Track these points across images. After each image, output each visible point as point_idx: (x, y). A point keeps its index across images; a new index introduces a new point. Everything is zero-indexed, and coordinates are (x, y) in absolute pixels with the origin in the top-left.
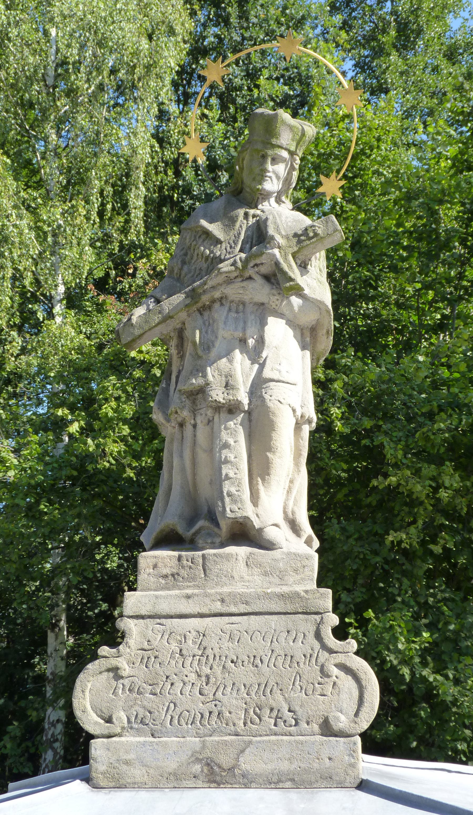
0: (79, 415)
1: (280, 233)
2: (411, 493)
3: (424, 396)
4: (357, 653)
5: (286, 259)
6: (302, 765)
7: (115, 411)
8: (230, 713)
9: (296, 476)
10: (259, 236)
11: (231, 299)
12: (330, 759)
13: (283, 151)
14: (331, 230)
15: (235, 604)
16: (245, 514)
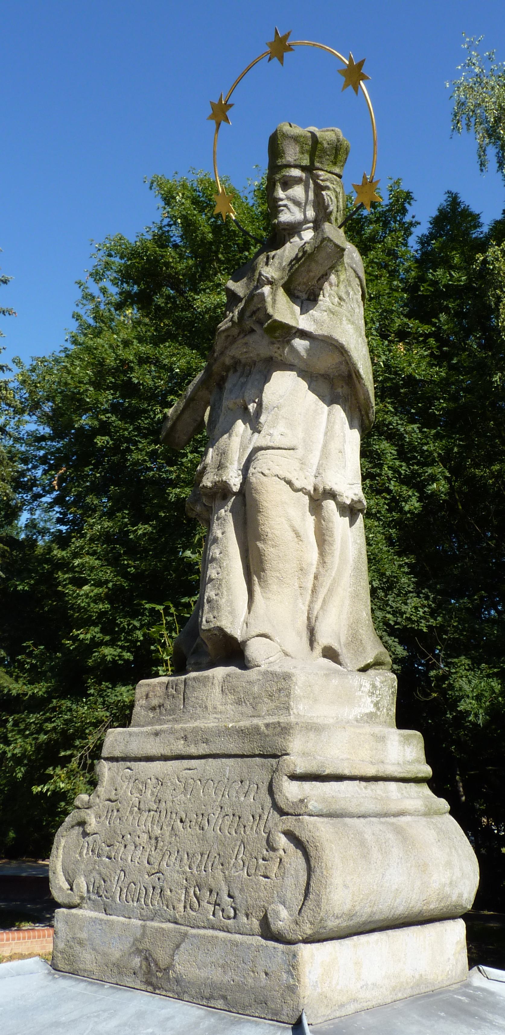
6: (236, 978)
8: (171, 891)
9: (321, 569)
11: (243, 361)
12: (266, 974)
13: (292, 169)
16: (218, 624)
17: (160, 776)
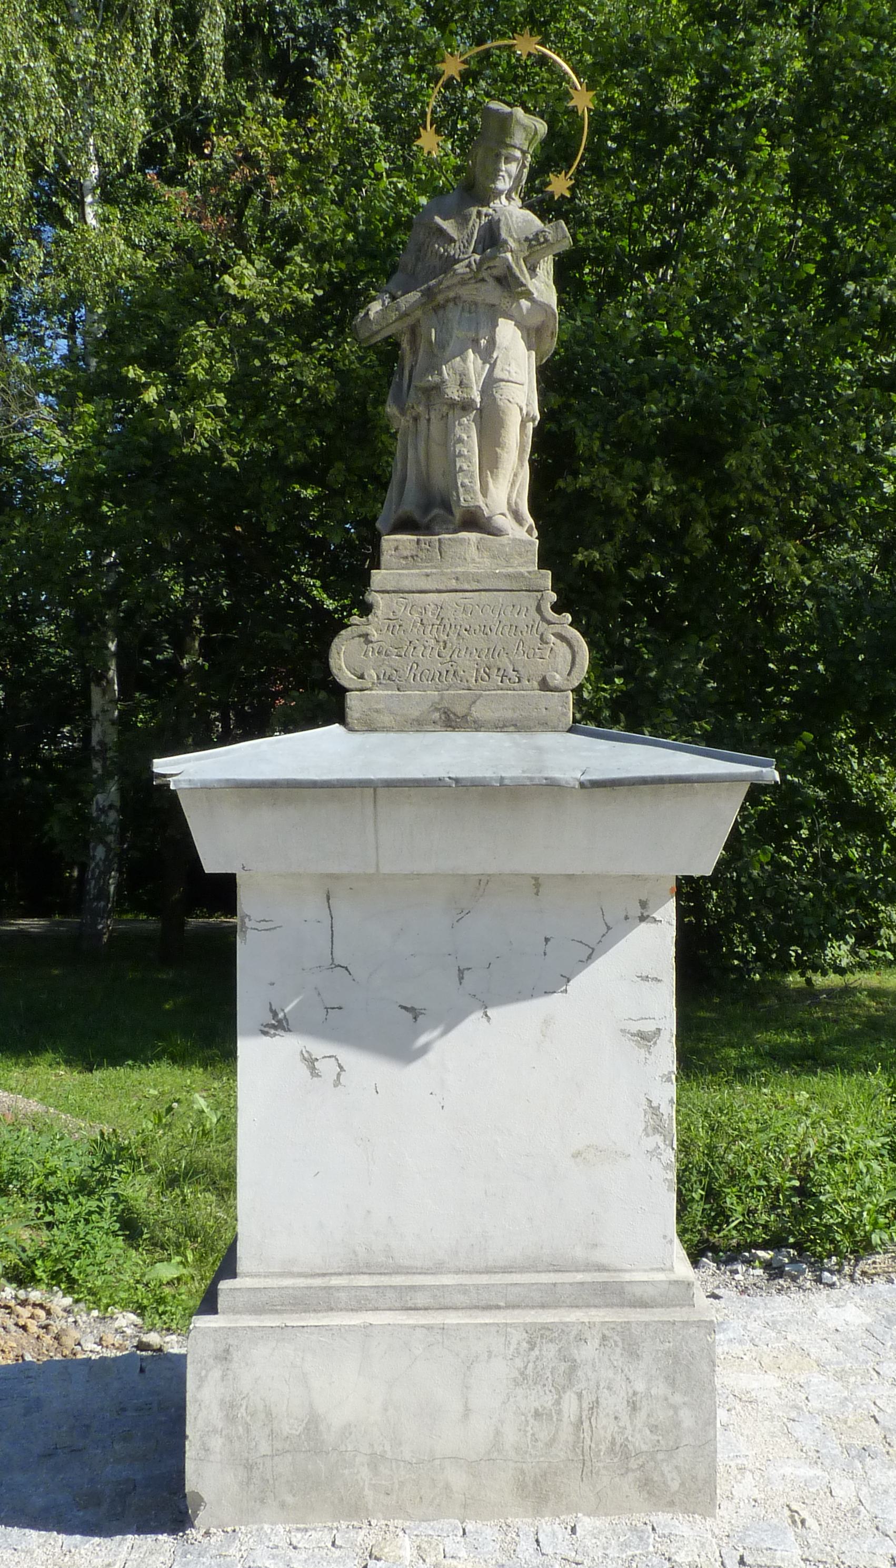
0: (155, 376)
1: (511, 236)
2: (608, 498)
3: (631, 361)
4: (571, 625)
5: (517, 264)
7: (208, 371)
10: (491, 238)
14: (560, 236)
15: (468, 582)
17: (439, 604)
